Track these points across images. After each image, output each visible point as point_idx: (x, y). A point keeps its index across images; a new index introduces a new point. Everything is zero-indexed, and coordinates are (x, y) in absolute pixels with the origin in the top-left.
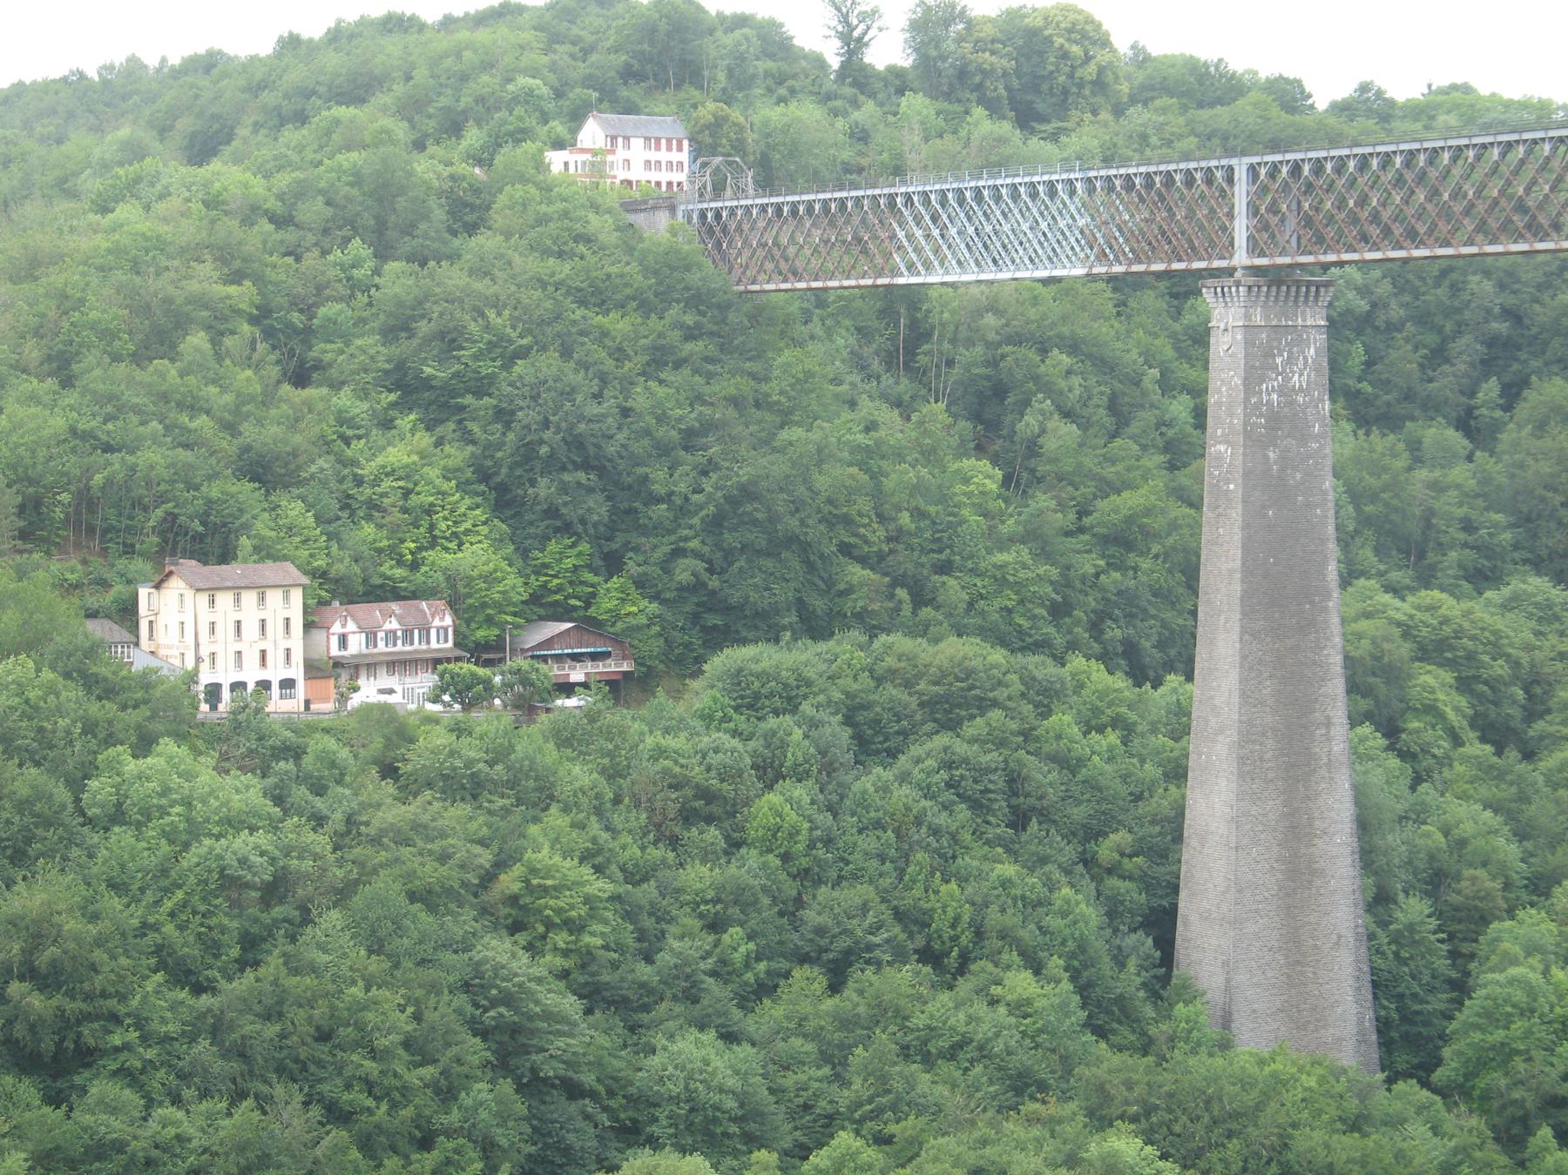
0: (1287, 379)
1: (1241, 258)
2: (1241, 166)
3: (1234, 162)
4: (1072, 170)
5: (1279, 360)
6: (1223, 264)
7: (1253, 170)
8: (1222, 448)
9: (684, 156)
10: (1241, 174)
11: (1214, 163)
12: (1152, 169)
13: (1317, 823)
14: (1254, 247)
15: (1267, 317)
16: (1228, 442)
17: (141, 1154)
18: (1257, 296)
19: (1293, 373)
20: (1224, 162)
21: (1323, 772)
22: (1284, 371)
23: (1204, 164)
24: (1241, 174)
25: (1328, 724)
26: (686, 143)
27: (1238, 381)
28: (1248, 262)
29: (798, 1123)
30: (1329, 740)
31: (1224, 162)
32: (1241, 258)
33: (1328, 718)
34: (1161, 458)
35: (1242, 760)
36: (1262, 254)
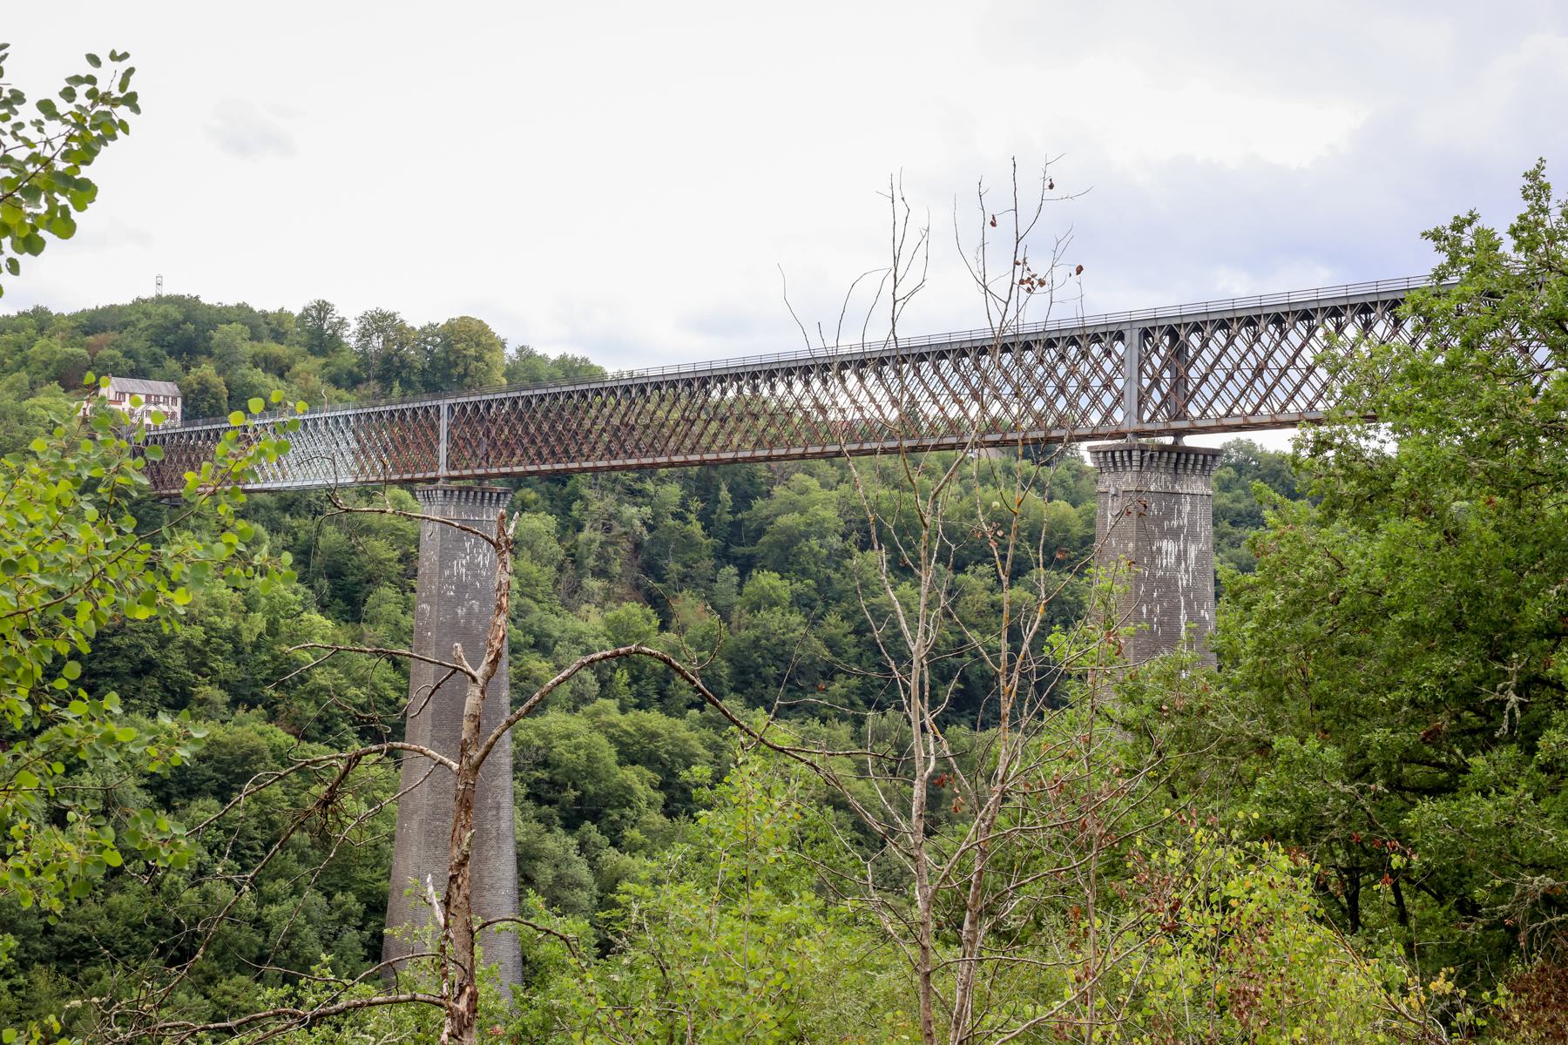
0: (473, 558)
1: (443, 471)
2: (444, 405)
3: (440, 402)
4: (347, 409)
5: (467, 545)
6: (433, 475)
7: (451, 408)
8: (424, 606)
9: (178, 409)
10: (444, 411)
11: (417, 405)
12: (394, 408)
13: (486, 880)
14: (452, 466)
15: (459, 513)
16: (428, 603)
17: (1452, 484)
18: (451, 498)
19: (479, 554)
20: (434, 403)
21: (493, 842)
22: (471, 552)
23: (411, 406)
24: (444, 411)
25: (498, 807)
26: (179, 401)
27: (435, 558)
28: (446, 473)
29: (1006, 708)
30: (499, 819)
31: (434, 403)
32: (443, 471)
33: (498, 803)
34: (248, 638)
35: (429, 833)
36: (455, 468)
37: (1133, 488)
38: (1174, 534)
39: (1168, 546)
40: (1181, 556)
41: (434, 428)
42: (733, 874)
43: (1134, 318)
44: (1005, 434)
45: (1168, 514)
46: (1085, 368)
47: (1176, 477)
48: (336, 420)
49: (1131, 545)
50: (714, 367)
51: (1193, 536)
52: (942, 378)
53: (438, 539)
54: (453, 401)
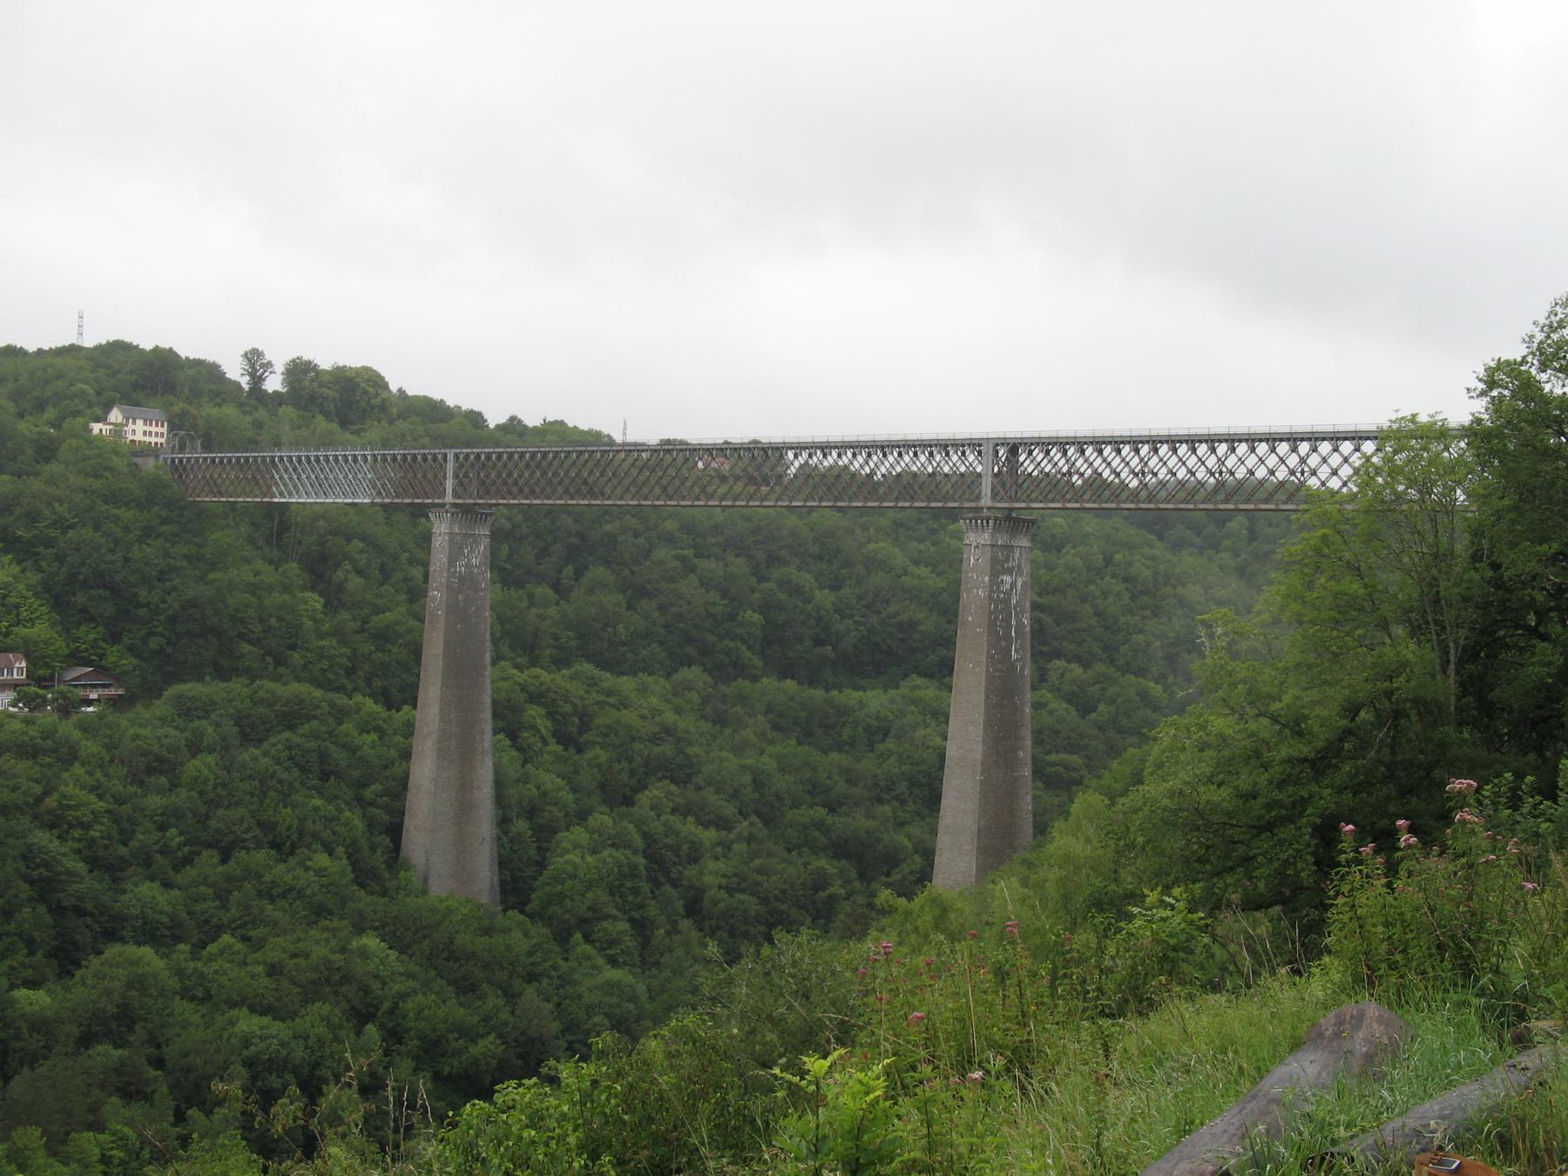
0: (469, 560)
1: (449, 499)
3: (447, 451)
6: (440, 501)
7: (456, 456)
10: (450, 457)
14: (455, 494)
20: (442, 451)
24: (450, 457)
30: (483, 741)
31: (442, 451)
32: (449, 499)
35: (439, 750)
36: (459, 498)
37: (988, 543)
38: (1010, 571)
39: (1007, 579)
40: (1013, 585)
41: (443, 468)
42: (1375, 882)
43: (990, 436)
44: (1277, 505)
45: (1007, 560)
46: (1335, 460)
47: (1013, 536)
48: (308, 458)
49: (987, 578)
50: (1024, 436)
51: (1020, 573)
52: (1105, 460)
53: (447, 547)
54: (458, 451)
